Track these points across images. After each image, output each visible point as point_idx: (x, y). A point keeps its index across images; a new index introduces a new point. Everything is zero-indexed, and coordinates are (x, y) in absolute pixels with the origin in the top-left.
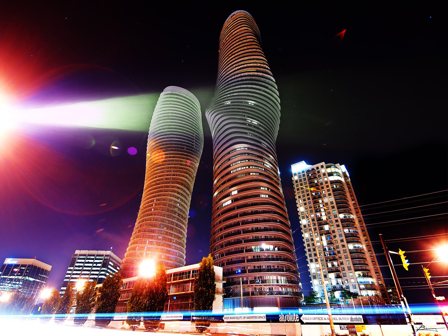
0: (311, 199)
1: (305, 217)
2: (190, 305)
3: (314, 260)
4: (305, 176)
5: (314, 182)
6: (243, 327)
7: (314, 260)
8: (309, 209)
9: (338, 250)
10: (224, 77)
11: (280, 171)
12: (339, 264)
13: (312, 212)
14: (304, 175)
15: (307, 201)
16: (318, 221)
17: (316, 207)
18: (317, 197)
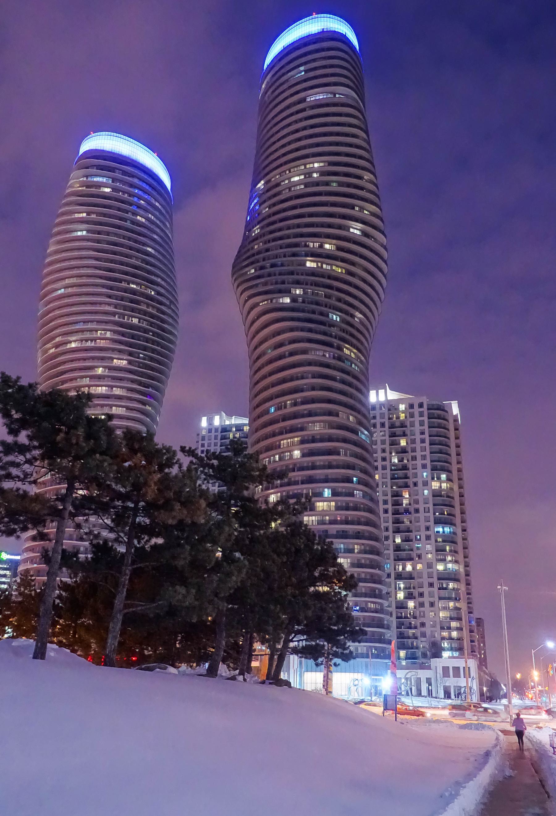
5: (400, 444)
9: (416, 506)
12: (409, 442)
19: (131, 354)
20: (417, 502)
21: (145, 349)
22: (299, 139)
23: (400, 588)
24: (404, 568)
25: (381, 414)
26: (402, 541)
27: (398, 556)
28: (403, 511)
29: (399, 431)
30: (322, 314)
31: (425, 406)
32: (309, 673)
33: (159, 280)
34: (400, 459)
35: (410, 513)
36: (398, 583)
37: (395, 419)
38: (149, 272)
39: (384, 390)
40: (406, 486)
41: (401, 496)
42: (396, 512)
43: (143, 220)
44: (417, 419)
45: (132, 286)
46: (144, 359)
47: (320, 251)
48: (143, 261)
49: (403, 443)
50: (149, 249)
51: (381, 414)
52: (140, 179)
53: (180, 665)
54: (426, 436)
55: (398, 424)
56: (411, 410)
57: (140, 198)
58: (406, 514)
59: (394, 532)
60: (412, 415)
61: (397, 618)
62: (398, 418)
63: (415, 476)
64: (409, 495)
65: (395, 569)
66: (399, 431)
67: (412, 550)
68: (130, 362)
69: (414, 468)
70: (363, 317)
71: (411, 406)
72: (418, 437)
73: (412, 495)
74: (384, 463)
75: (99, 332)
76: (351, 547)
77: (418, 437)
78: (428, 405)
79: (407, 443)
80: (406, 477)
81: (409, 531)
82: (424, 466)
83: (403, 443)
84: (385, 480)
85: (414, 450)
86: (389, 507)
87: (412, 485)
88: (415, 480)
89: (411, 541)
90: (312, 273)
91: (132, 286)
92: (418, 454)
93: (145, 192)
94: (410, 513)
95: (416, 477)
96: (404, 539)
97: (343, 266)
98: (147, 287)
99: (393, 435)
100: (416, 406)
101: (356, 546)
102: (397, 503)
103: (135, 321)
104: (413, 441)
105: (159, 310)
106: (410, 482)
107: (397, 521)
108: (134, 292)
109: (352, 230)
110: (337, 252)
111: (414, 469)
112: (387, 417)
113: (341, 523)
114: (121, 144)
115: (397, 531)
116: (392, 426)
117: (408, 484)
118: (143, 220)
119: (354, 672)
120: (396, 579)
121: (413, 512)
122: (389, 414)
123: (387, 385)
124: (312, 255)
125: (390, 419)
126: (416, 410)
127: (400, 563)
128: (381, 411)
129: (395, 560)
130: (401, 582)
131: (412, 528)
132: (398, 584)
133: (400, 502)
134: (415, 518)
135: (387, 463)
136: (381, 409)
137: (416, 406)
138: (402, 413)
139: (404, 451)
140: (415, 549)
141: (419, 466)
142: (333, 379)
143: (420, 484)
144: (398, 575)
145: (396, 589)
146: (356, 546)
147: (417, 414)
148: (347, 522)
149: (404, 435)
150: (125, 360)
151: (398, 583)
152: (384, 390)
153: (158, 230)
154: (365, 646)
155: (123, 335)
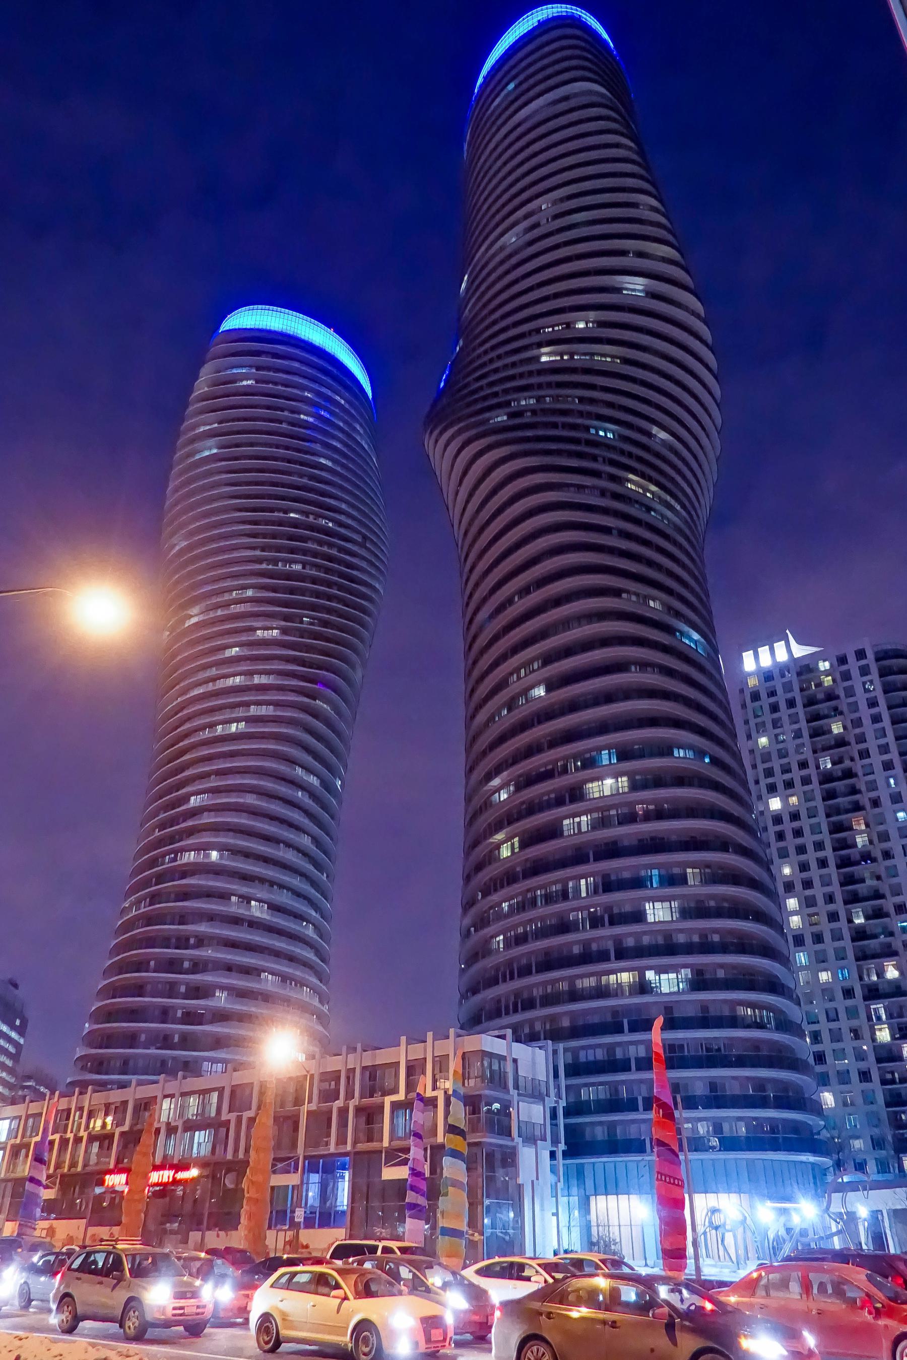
0: (815, 779)
1: (833, 1079)
2: (305, 418)
3: (780, 786)
4: (791, 690)
5: (830, 731)
6: (477, 128)
7: (780, 786)
8: (823, 908)
9: (885, 845)
10: (484, 221)
11: (605, 40)
12: (849, 725)
13: (818, 831)
14: (788, 687)
15: (815, 873)
16: (892, 1107)
17: (809, 687)
18: (840, 774)
19: (286, 618)
20: (884, 837)
21: (314, 607)
22: (500, 156)
23: (879, 1018)
24: (881, 974)
25: (784, 684)
26: (867, 918)
27: (864, 952)
28: (858, 857)
29: (823, 708)
30: (613, 478)
31: (870, 655)
32: (601, 1199)
33: (344, 506)
34: (836, 758)
35: (874, 860)
36: (872, 1007)
37: (813, 688)
38: (323, 494)
39: (783, 642)
40: (857, 807)
41: (850, 828)
42: (844, 863)
43: (311, 420)
44: (857, 681)
45: (292, 515)
46: (311, 624)
47: (569, 335)
48: (312, 477)
49: (837, 728)
50: (323, 461)
51: (784, 684)
52: (301, 362)
53: (173, 1188)
54: (882, 708)
55: (820, 696)
56: (844, 668)
57: (304, 388)
58: (866, 863)
59: (846, 903)
60: (846, 676)
61: (884, 1082)
62: (819, 685)
63: (872, 786)
64: (867, 825)
65: (861, 978)
66: (823, 708)
67: (891, 934)
68: (284, 631)
69: (869, 771)
70: (671, 438)
71: (842, 660)
72: (865, 713)
73: (871, 825)
74: (804, 772)
75: (235, 592)
76: (676, 871)
77: (865, 713)
78: (876, 653)
79: (845, 728)
80: (854, 791)
81: (878, 895)
82: (888, 766)
83: (837, 728)
84: (812, 804)
85: (861, 739)
86: (828, 853)
87: (868, 805)
88: (873, 794)
89: (887, 915)
90: (552, 369)
91: (292, 515)
92: (872, 744)
93: (314, 380)
94: (874, 860)
95: (876, 789)
96: (870, 912)
97: (614, 353)
98: (318, 516)
99: (814, 718)
100: (851, 658)
101: (689, 870)
102: (843, 845)
103: (297, 567)
104: (858, 723)
105: (341, 549)
106: (864, 799)
107: (849, 880)
108: (295, 524)
109: (625, 292)
110: (600, 329)
111: (868, 774)
112: (796, 687)
113: (648, 817)
114: (270, 318)
115: (853, 899)
116: (811, 702)
117: (861, 804)
118: (311, 420)
119: (706, 1192)
120: (865, 999)
121: (880, 857)
122: (801, 682)
123: (787, 631)
124: (549, 343)
125: (802, 690)
126: (853, 665)
127: (872, 964)
128: (784, 680)
129: (857, 959)
130: (878, 1006)
131: (885, 889)
132: (875, 1009)
133: (849, 842)
134: (887, 868)
135: (811, 771)
136: (783, 676)
137: (851, 658)
138: (827, 676)
139: (841, 742)
140: (897, 932)
141: (878, 768)
142: (607, 530)
143: (885, 800)
144: (870, 990)
145: (870, 1018)
146: (689, 870)
147: (855, 673)
148: (659, 815)
149: (837, 712)
150: (276, 628)
151: (872, 1007)
152: (783, 642)
153: (340, 435)
154: (740, 1119)
155: (274, 589)
